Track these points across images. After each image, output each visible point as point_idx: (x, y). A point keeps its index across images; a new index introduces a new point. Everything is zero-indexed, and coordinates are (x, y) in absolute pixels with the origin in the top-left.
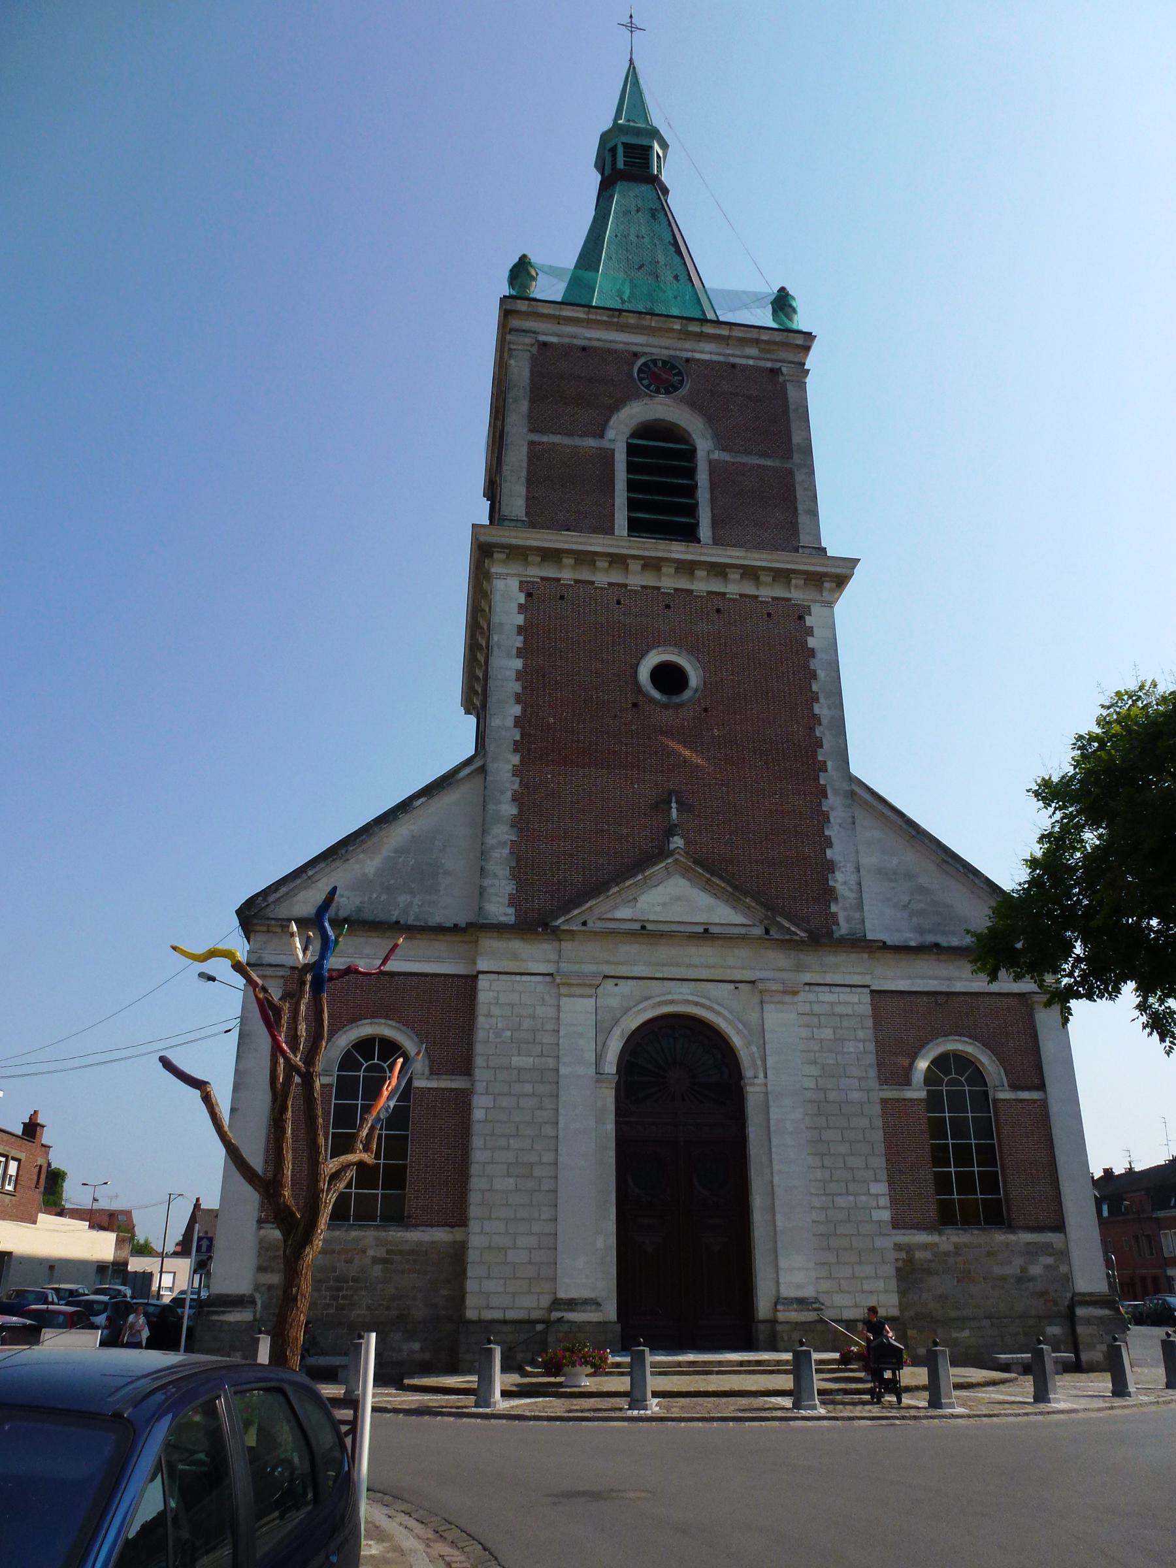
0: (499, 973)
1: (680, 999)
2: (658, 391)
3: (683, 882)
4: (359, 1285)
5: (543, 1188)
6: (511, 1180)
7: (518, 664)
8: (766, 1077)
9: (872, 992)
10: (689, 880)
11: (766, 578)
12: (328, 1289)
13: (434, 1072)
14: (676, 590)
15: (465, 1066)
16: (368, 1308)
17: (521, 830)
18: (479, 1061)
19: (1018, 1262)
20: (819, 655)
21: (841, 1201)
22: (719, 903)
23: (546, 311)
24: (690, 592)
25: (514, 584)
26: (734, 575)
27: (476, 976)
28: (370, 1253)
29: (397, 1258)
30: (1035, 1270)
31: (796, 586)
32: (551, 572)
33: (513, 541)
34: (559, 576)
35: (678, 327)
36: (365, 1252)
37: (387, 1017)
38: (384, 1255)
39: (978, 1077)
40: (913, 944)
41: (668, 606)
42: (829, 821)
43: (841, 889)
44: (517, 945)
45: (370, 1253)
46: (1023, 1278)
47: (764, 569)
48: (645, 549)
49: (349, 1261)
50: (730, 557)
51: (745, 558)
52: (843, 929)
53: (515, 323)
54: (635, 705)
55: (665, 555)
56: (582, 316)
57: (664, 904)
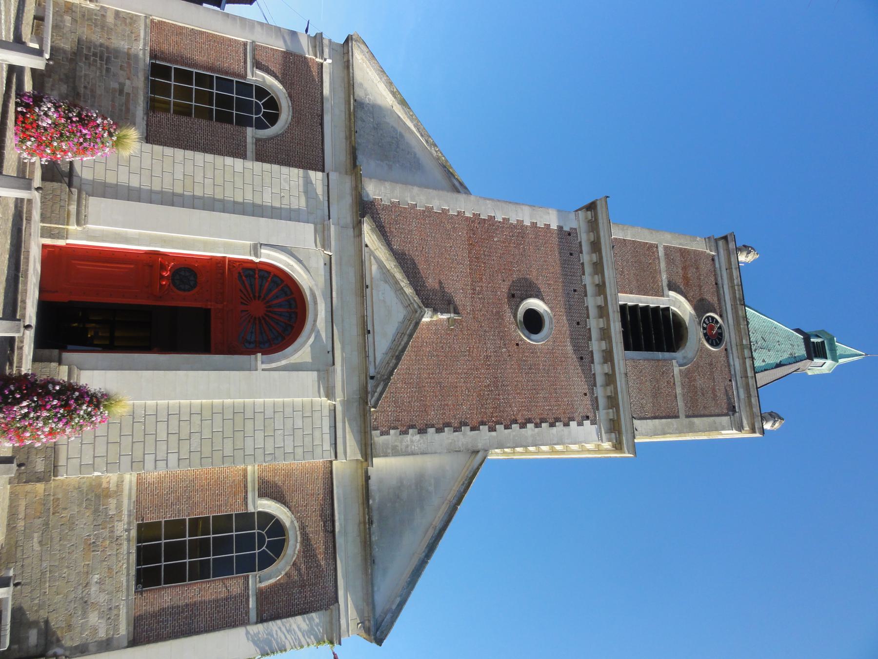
0: (328, 186)
2: (704, 329)
4: (104, 72)
6: (181, 177)
7: (527, 223)
8: (263, 370)
9: (331, 462)
11: (609, 390)
12: (102, 52)
13: (258, 141)
14: (590, 329)
16: (86, 75)
19: (103, 598)
20: (566, 429)
21: (162, 427)
22: (390, 341)
23: (732, 260)
24: (590, 339)
25: (574, 225)
26: (607, 368)
27: (323, 171)
28: (128, 82)
29: (124, 98)
30: (93, 618)
31: (608, 414)
32: (585, 248)
33: (600, 221)
34: (584, 252)
35: (744, 342)
36: (128, 79)
37: (293, 117)
38: (126, 91)
39: (266, 562)
40: (371, 502)
41: (578, 323)
45: (128, 82)
46: (85, 604)
47: (616, 388)
48: (612, 305)
49: (121, 68)
50: (619, 363)
51: (620, 373)
52: (379, 439)
53: (721, 243)
54: (513, 296)
55: (611, 318)
56: (735, 282)
57: (384, 301)
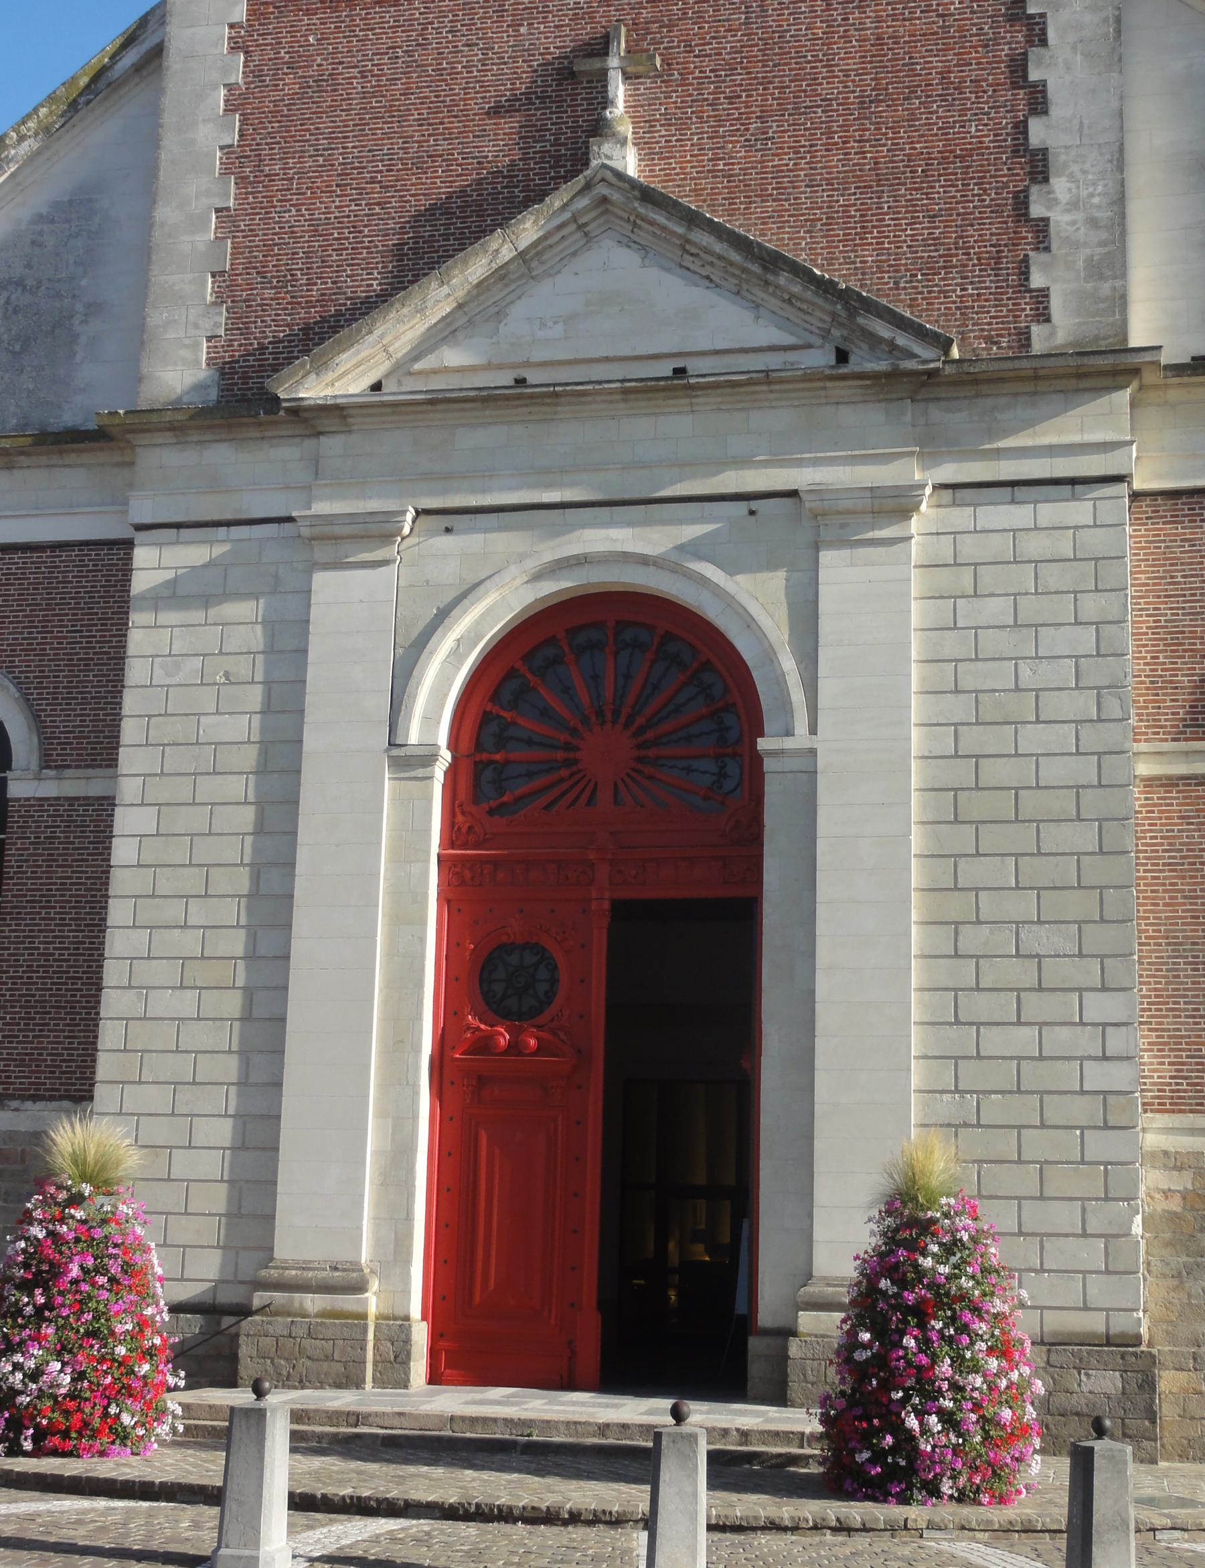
1: (624, 548)
3: (626, 258)
5: (255, 1015)
8: (813, 730)
10: (644, 249)
13: (49, 761)
15: (101, 749)
17: (242, 181)
18: (130, 731)
22: (711, 296)
27: (128, 544)
42: (1044, 42)
43: (1061, 221)
44: (222, 456)
